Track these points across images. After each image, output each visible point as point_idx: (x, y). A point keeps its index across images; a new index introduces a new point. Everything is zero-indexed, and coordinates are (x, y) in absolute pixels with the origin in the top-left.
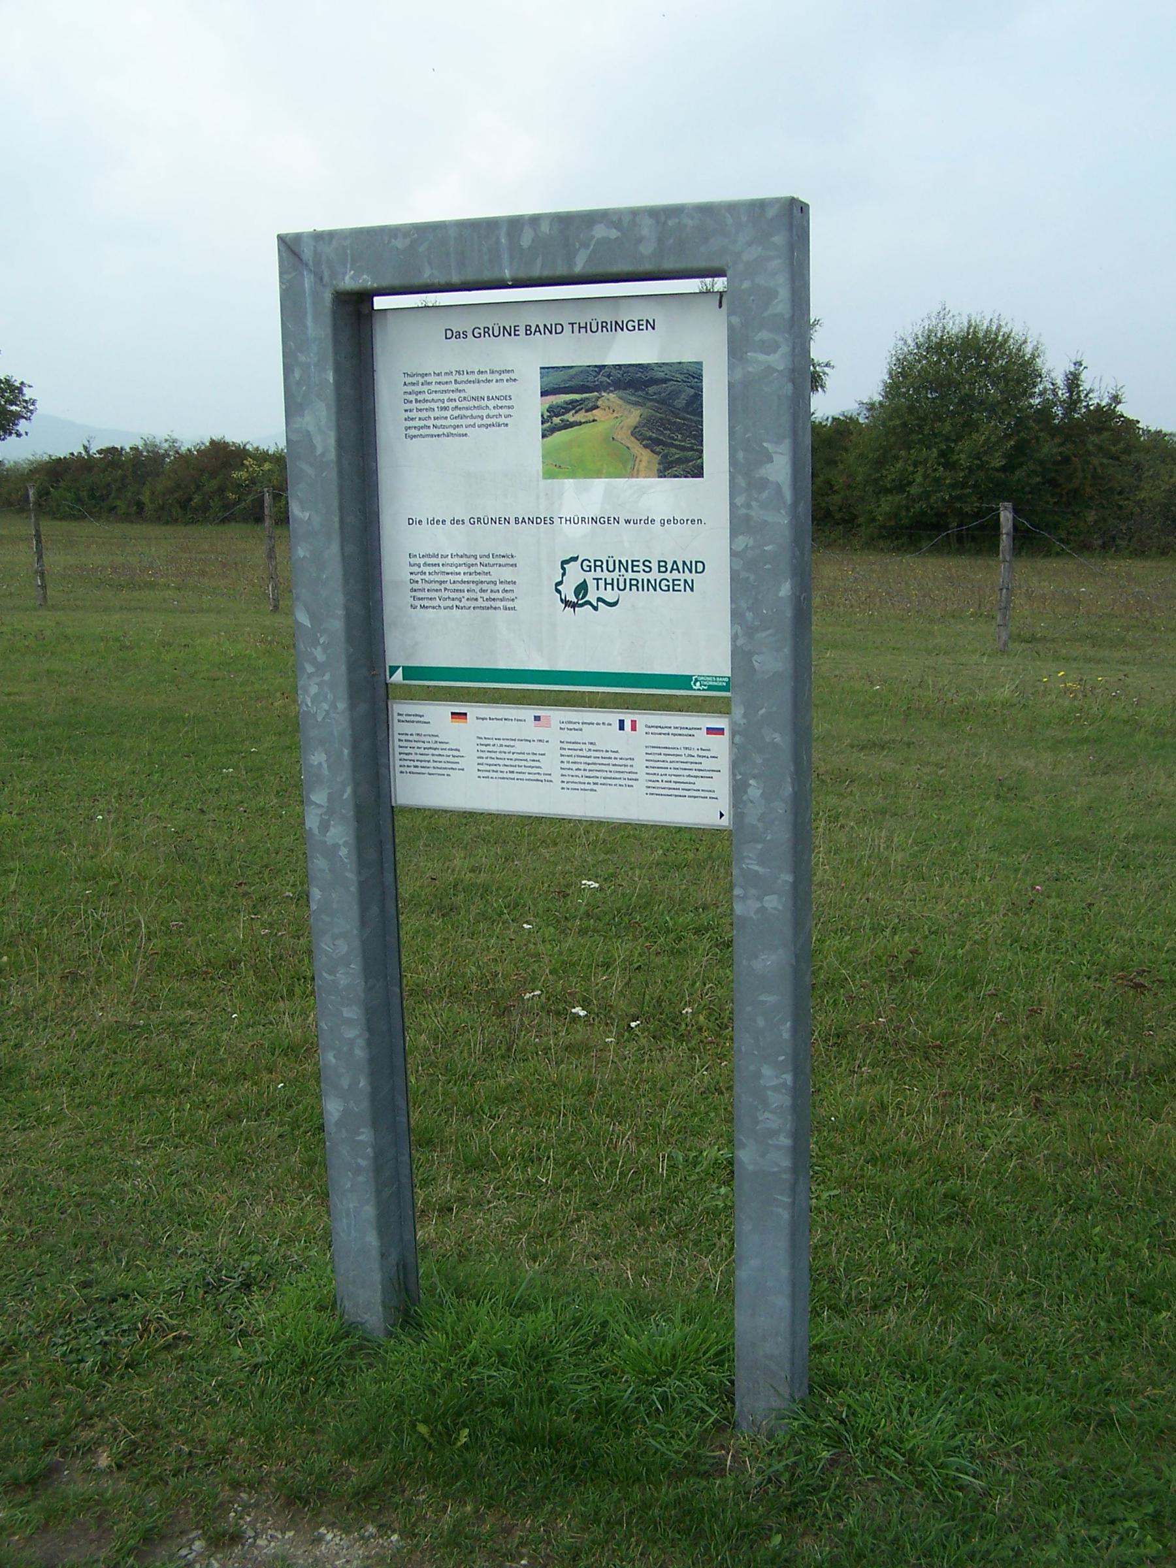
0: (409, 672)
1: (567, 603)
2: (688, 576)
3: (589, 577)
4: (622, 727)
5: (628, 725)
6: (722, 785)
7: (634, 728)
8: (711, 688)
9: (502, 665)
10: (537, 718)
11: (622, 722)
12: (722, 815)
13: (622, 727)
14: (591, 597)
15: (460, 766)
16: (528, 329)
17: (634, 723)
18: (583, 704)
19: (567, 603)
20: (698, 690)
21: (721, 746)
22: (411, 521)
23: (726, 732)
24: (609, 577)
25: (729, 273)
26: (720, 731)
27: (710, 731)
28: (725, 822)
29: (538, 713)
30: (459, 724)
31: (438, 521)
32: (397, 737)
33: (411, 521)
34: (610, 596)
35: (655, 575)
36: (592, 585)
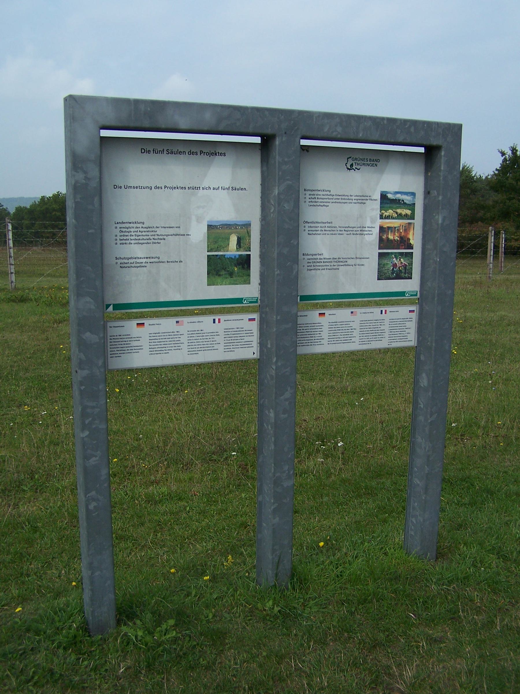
0: (117, 307)
1: (348, 169)
2: (376, 163)
3: (354, 162)
4: (214, 322)
5: (217, 321)
6: (255, 339)
7: (219, 322)
8: (251, 302)
9: (340, 292)
10: (177, 322)
11: (214, 320)
12: (254, 353)
13: (214, 322)
14: (354, 167)
15: (150, 347)
16: (165, 187)
17: (219, 320)
18: (197, 314)
19: (348, 169)
20: (245, 304)
21: (254, 326)
22: (110, 327)
23: (256, 320)
24: (358, 162)
25: (299, 148)
26: (254, 320)
27: (410, 311)
28: (255, 356)
29: (177, 320)
30: (141, 329)
31: (242, 189)
32: (109, 338)
33: (110, 327)
34: (358, 167)
35: (369, 162)
36: (354, 164)
